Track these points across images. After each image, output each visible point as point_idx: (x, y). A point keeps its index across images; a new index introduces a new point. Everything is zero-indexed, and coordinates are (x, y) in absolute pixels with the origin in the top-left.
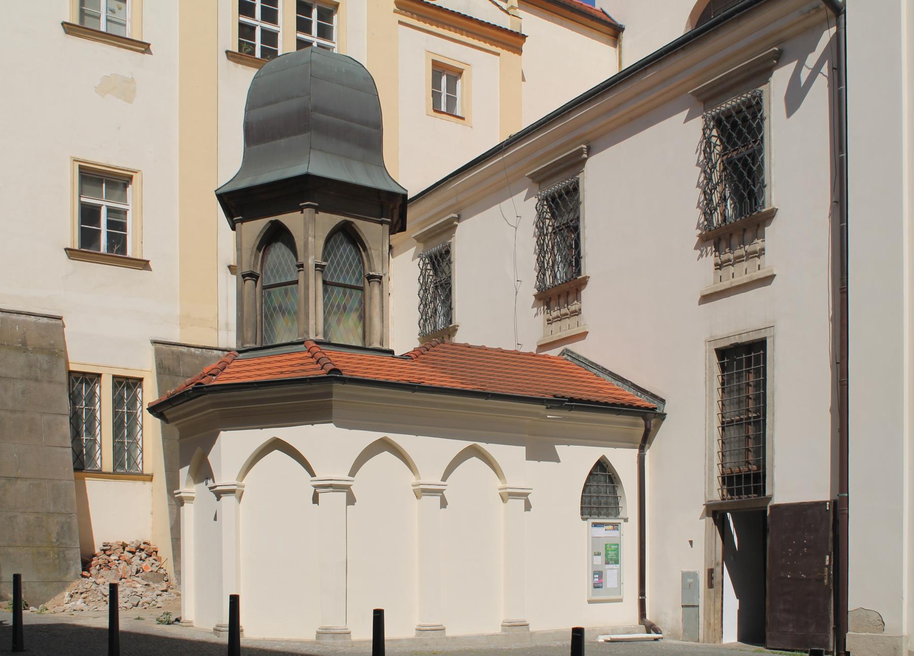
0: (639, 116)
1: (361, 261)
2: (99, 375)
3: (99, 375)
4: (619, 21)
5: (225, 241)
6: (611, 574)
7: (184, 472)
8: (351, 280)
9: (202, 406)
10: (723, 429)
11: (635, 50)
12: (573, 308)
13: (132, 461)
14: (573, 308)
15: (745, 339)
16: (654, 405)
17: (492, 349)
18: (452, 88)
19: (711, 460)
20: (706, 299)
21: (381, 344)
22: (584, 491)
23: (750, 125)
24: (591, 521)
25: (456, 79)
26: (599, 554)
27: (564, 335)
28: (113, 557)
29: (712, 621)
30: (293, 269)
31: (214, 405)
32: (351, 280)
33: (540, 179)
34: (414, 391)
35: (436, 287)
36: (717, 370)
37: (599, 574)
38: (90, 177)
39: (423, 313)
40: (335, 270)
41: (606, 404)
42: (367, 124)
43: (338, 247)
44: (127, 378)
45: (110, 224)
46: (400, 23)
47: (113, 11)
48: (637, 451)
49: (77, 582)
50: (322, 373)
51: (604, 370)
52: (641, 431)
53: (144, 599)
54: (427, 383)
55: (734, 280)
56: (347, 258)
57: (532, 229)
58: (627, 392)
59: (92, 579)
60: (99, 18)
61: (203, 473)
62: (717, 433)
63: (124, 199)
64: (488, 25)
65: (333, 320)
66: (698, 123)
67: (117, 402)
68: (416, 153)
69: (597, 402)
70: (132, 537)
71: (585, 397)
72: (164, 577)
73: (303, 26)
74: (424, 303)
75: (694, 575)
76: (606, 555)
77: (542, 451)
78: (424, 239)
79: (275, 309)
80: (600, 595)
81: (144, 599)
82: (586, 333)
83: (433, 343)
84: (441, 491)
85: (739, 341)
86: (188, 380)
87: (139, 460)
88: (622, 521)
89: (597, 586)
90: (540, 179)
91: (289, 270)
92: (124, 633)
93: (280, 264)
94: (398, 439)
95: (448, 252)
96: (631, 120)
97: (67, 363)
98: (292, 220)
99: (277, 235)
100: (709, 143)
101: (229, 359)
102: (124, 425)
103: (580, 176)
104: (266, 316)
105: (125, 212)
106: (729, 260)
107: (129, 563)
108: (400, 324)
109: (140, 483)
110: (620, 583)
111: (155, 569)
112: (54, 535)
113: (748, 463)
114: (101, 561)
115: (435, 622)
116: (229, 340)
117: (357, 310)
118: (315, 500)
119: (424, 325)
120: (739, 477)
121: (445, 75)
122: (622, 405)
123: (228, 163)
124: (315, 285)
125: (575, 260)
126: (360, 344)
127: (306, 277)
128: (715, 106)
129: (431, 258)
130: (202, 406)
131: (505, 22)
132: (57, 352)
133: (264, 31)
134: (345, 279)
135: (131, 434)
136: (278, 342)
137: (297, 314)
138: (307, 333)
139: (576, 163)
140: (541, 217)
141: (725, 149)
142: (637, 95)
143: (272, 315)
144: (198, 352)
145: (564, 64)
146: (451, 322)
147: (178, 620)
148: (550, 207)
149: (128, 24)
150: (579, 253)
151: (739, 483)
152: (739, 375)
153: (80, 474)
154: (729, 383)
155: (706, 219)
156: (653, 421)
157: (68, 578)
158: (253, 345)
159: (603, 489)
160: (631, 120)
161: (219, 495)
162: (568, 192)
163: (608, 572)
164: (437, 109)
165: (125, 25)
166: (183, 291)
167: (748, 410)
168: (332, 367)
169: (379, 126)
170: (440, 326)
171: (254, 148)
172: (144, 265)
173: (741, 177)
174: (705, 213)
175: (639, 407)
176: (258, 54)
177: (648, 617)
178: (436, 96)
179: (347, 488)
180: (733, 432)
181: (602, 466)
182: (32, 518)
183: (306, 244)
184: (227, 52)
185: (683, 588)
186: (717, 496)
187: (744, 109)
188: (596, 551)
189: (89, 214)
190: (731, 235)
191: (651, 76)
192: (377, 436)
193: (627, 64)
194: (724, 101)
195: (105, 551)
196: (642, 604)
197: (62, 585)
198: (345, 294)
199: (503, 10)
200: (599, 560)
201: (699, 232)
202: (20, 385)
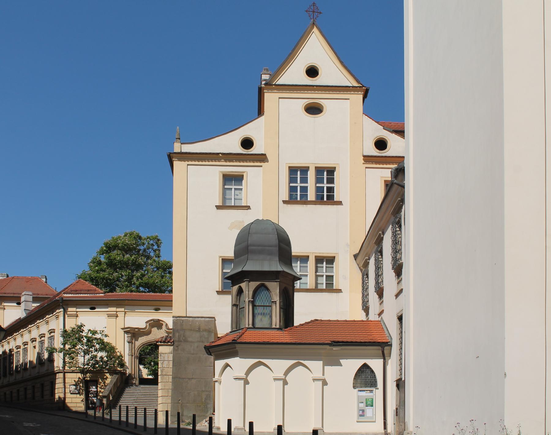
6: (369, 411)
26: (362, 403)
37: (363, 411)
47: (237, 195)
76: (366, 403)
80: (362, 419)
92: (198, 431)
112: (204, 399)
200: (362, 405)
202: (196, 344)
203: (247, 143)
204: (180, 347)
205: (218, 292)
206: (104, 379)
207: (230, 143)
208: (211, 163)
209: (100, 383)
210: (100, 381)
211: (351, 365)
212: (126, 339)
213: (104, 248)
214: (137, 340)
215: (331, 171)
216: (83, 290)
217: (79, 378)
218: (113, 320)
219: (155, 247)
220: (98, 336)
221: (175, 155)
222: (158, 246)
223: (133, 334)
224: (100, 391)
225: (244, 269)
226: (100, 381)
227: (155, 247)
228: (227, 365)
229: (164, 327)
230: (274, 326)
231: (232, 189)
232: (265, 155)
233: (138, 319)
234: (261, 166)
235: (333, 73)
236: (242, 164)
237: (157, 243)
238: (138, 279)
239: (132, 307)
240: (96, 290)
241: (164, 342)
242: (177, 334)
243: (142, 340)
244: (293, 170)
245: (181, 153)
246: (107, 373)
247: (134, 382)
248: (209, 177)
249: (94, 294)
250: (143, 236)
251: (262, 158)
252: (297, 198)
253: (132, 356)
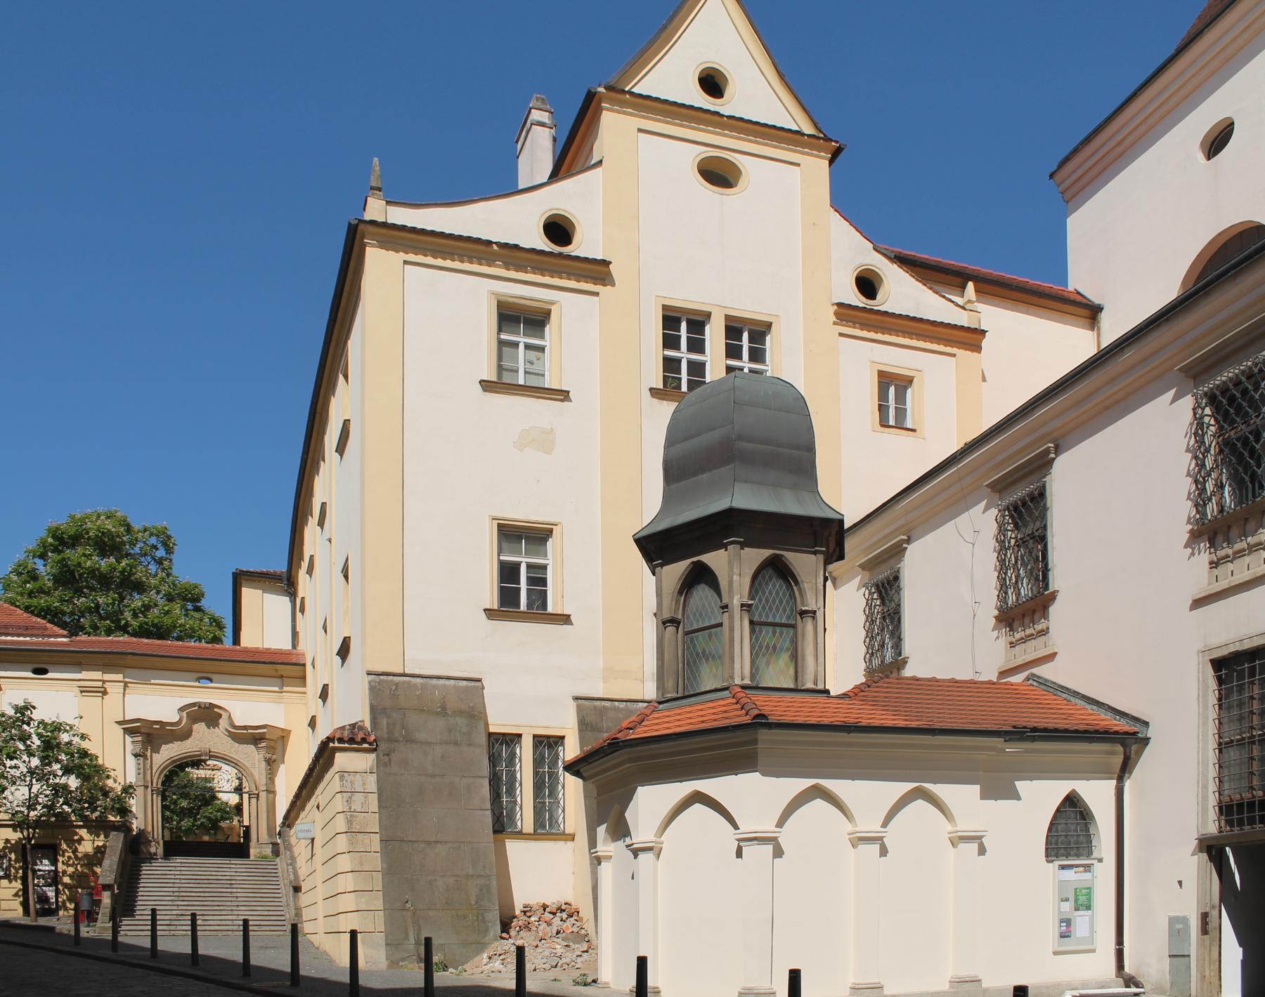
0: (1117, 402)
1: (793, 596)
2: (520, 736)
3: (520, 736)
4: (1097, 301)
5: (646, 587)
6: (1081, 922)
7: (601, 830)
8: (781, 618)
9: (620, 759)
10: (1220, 751)
11: (1114, 327)
12: (1039, 627)
13: (553, 821)
14: (1039, 627)
15: (1247, 645)
16: (1136, 729)
17: (944, 681)
18: (901, 398)
19: (1205, 787)
20: (1198, 603)
21: (816, 683)
22: (1050, 830)
23: (1252, 397)
24: (1057, 863)
25: (906, 388)
26: (1067, 900)
27: (1029, 658)
28: (533, 919)
29: (1207, 973)
30: (717, 610)
31: (631, 760)
32: (781, 618)
33: (1000, 487)
34: (849, 732)
35: (884, 618)
36: (1212, 684)
37: (1068, 922)
38: (510, 534)
39: (869, 647)
40: (764, 608)
41: (1077, 731)
42: (797, 447)
43: (767, 583)
44: (548, 737)
45: (531, 581)
46: (841, 335)
48: (1114, 782)
49: (496, 944)
50: (746, 719)
51: (1076, 694)
52: (1119, 759)
53: (564, 960)
54: (864, 722)
56: (777, 594)
57: (993, 544)
58: (1103, 716)
59: (511, 941)
60: (517, 371)
61: (620, 830)
62: (1212, 756)
64: (942, 324)
65: (762, 661)
66: (1188, 402)
67: (538, 762)
68: (856, 472)
69: (1066, 731)
70: (552, 899)
71: (1050, 726)
72: (585, 938)
73: (733, 351)
74: (870, 635)
75: (1185, 920)
76: (1076, 901)
77: (999, 788)
78: (868, 566)
79: (698, 654)
80: (1068, 945)
81: (564, 960)
82: (1055, 654)
83: (876, 679)
84: (881, 839)
86: (605, 735)
87: (561, 819)
88: (1095, 862)
89: (1063, 936)
90: (1000, 487)
91: (713, 612)
93: (704, 606)
94: (829, 784)
95: (896, 578)
96: (1107, 408)
97: (487, 725)
98: (715, 560)
99: (701, 576)
100: (1200, 424)
101: (648, 712)
102: (545, 786)
103: (1047, 479)
104: (689, 664)
105: (544, 567)
106: (1228, 556)
107: (549, 924)
108: (841, 659)
109: (561, 843)
110: (1092, 931)
111: (576, 929)
113: (1252, 788)
114: (520, 923)
115: (871, 979)
116: (650, 691)
117: (788, 649)
118: (739, 854)
119: (870, 660)
120: (1240, 806)
121: (892, 385)
122: (1096, 732)
123: (647, 504)
124: (741, 627)
125: (1041, 572)
126: (792, 686)
127: (731, 618)
128: (1208, 381)
129: (877, 586)
130: (620, 759)
131: (961, 318)
132: (476, 714)
133: (690, 363)
134: (774, 617)
135: (553, 794)
136: (703, 690)
137: (723, 658)
138: (732, 677)
139: (1043, 464)
140: (1002, 529)
141: (1221, 428)
142: (1113, 380)
143: (695, 662)
144: (622, 705)
145: (1029, 353)
146: (900, 654)
147: (594, 981)
148: (1011, 516)
149: (547, 374)
150: (1047, 565)
151: (1240, 812)
152: (1241, 689)
153: (499, 836)
154: (1227, 697)
155: (1198, 512)
156: (1134, 748)
157: (487, 939)
158: (674, 695)
159: (1073, 827)
160: (1107, 408)
161: (636, 853)
162: (1033, 499)
163: (1078, 919)
164: (884, 424)
166: (603, 644)
167: (1252, 728)
168: (757, 712)
169: (811, 449)
170: (888, 659)
171: (674, 486)
172: (565, 619)
173: (1240, 458)
174: (1196, 505)
175: (1116, 733)
176: (684, 388)
177: (1127, 969)
178: (883, 409)
179: (775, 839)
180: (1233, 754)
181: (1072, 801)
182: (451, 881)
183: (731, 583)
184: (651, 389)
185: (1171, 935)
186: (1212, 828)
187: (1244, 379)
188: (1065, 896)
189: (508, 573)
190: (1229, 527)
191: (1129, 355)
192: (808, 782)
193: (1105, 343)
194: (1220, 373)
195: (525, 912)
196: (1120, 954)
197: (482, 947)
198: (774, 633)
199: (957, 305)
200: (1067, 907)
201: (1190, 527)
203: (558, 230)
204: (394, 757)
205: (490, 613)
206: (74, 842)
207: (515, 220)
208: (466, 266)
209: (64, 851)
210: (64, 846)
211: (1041, 797)
212: (129, 747)
213: (50, 540)
214: (156, 750)
215: (760, 332)
216: (13, 627)
217: (7, 841)
218: (96, 700)
219: (161, 553)
220: (65, 737)
221: (371, 228)
222: (169, 550)
223: (148, 735)
224: (64, 872)
226: (64, 846)
227: (161, 553)
229: (223, 723)
231: (516, 345)
232: (605, 263)
233: (161, 701)
234: (597, 294)
235: (757, 93)
236: (547, 280)
237: (165, 545)
238: (135, 616)
239: (143, 672)
240: (46, 629)
241: (352, 741)
242: (384, 722)
243: (169, 752)
244: (671, 320)
245: (385, 225)
246: (80, 827)
247: (153, 850)
248: (471, 297)
249: (44, 636)
250: (136, 526)
251: (597, 272)
252: (679, 387)
253: (146, 787)
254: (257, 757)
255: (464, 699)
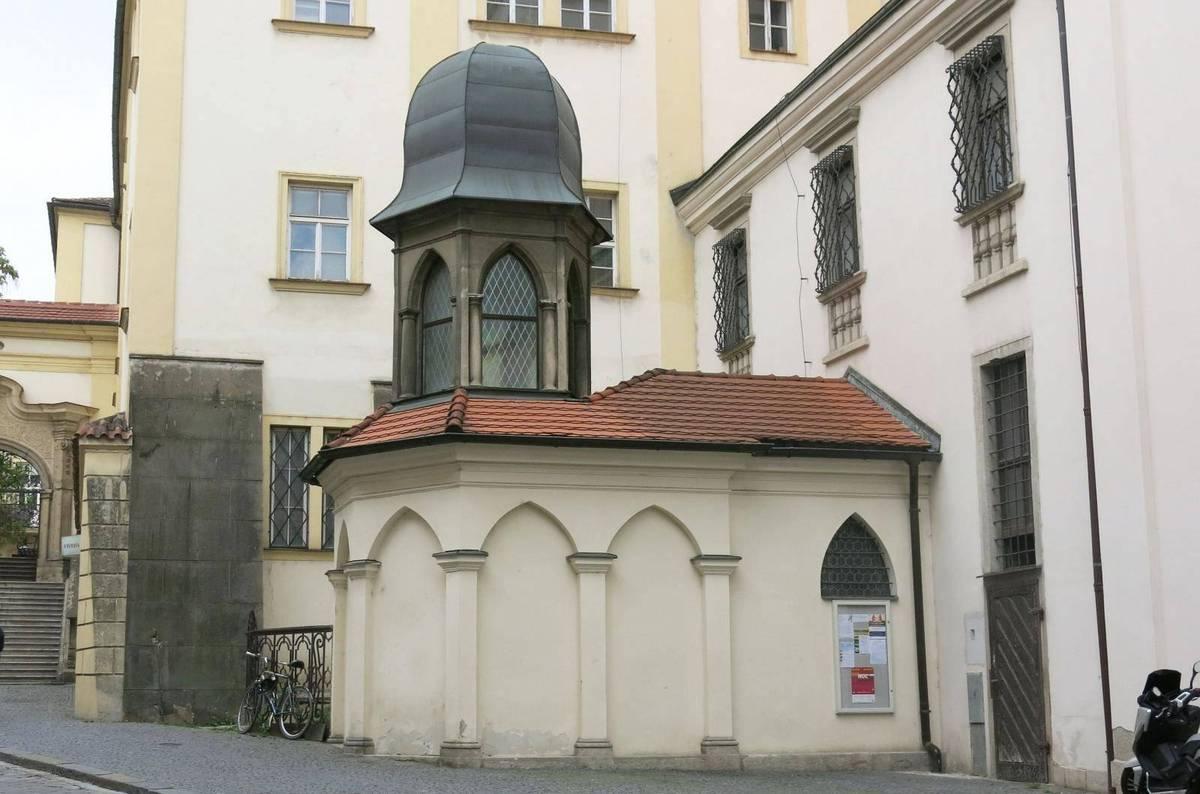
2: (308, 429)
3: (308, 429)
16: (928, 442)
21: (556, 385)
24: (836, 603)
55: (991, 276)
63: (344, 215)
85: (999, 356)
99: (433, 266)
127: (459, 313)
132: (251, 404)
138: (458, 378)
164: (756, 46)
165: (348, 6)
225: (457, 193)
228: (406, 515)
230: (550, 387)
241: (104, 436)
254: (54, 445)
255: (237, 388)
